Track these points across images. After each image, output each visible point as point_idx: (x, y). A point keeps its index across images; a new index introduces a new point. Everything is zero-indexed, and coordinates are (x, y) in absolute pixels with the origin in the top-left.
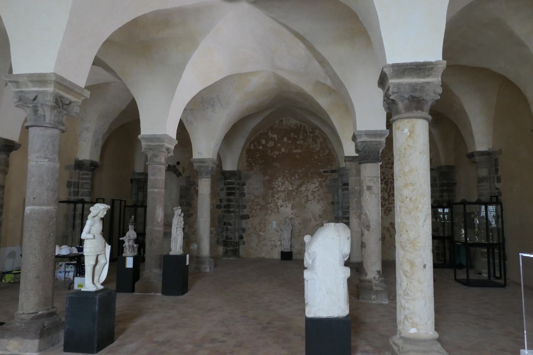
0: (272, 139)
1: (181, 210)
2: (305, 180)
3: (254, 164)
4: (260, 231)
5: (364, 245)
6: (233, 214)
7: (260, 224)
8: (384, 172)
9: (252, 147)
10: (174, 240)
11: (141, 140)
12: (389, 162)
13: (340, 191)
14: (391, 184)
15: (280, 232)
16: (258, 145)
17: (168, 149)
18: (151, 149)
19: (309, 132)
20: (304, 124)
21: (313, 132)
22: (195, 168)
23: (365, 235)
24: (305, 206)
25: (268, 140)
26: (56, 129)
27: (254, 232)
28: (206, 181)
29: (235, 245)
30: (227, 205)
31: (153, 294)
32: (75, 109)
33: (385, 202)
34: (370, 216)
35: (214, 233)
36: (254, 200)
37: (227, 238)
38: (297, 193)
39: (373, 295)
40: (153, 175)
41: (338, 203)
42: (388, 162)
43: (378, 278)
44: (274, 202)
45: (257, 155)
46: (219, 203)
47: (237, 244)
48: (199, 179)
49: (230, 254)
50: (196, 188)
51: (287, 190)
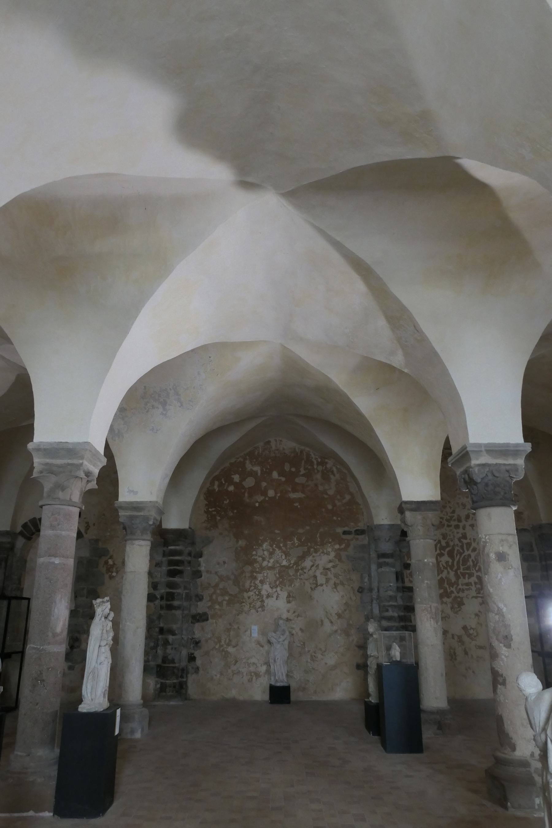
0: (252, 474)
1: (111, 604)
3: (218, 518)
4: (228, 645)
5: (500, 680)
6: (178, 613)
7: (228, 630)
9: (216, 488)
10: (91, 677)
11: (34, 454)
13: (374, 567)
15: (266, 647)
16: (227, 484)
17: (88, 474)
18: (52, 472)
19: (315, 462)
20: (307, 449)
21: (322, 463)
22: (121, 520)
23: (503, 657)
24: (311, 596)
25: (245, 474)
27: (217, 647)
29: (180, 674)
30: (168, 593)
31: (31, 813)
33: (452, 589)
34: (510, 616)
36: (217, 585)
37: (165, 659)
38: (297, 571)
40: (52, 527)
41: (371, 590)
42: (452, 517)
44: (254, 589)
45: (225, 502)
47: (184, 672)
48: (129, 542)
49: (171, 693)
50: (108, 562)
51: (278, 565)
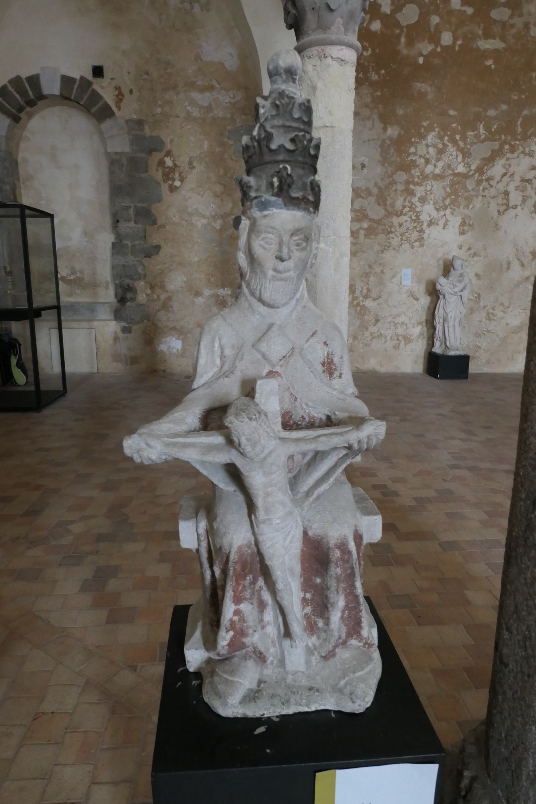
2: (505, 142)
38: (479, 182)
51: (450, 172)
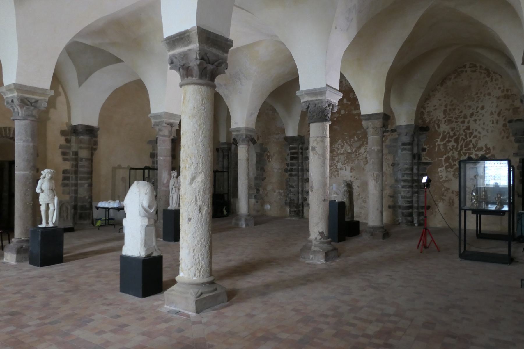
8: (455, 127)
12: (460, 115)
13: (400, 151)
14: (462, 142)
26: (27, 120)
28: (243, 148)
32: (43, 105)
33: (455, 163)
35: (283, 195)
38: (356, 155)
39: (311, 255)
43: (320, 239)
46: (286, 167)
51: (346, 152)
